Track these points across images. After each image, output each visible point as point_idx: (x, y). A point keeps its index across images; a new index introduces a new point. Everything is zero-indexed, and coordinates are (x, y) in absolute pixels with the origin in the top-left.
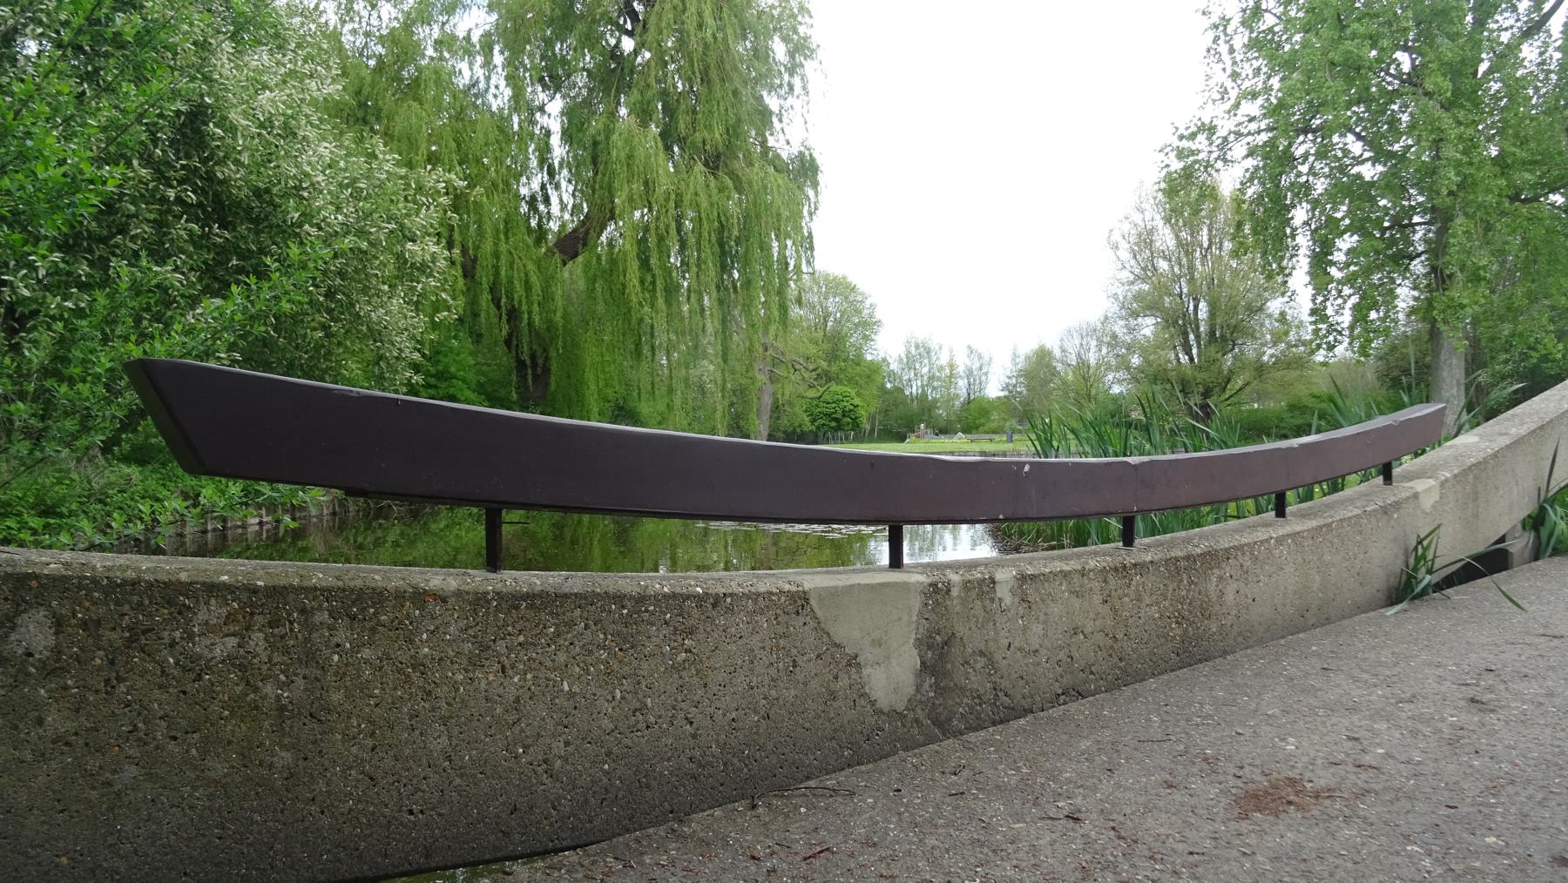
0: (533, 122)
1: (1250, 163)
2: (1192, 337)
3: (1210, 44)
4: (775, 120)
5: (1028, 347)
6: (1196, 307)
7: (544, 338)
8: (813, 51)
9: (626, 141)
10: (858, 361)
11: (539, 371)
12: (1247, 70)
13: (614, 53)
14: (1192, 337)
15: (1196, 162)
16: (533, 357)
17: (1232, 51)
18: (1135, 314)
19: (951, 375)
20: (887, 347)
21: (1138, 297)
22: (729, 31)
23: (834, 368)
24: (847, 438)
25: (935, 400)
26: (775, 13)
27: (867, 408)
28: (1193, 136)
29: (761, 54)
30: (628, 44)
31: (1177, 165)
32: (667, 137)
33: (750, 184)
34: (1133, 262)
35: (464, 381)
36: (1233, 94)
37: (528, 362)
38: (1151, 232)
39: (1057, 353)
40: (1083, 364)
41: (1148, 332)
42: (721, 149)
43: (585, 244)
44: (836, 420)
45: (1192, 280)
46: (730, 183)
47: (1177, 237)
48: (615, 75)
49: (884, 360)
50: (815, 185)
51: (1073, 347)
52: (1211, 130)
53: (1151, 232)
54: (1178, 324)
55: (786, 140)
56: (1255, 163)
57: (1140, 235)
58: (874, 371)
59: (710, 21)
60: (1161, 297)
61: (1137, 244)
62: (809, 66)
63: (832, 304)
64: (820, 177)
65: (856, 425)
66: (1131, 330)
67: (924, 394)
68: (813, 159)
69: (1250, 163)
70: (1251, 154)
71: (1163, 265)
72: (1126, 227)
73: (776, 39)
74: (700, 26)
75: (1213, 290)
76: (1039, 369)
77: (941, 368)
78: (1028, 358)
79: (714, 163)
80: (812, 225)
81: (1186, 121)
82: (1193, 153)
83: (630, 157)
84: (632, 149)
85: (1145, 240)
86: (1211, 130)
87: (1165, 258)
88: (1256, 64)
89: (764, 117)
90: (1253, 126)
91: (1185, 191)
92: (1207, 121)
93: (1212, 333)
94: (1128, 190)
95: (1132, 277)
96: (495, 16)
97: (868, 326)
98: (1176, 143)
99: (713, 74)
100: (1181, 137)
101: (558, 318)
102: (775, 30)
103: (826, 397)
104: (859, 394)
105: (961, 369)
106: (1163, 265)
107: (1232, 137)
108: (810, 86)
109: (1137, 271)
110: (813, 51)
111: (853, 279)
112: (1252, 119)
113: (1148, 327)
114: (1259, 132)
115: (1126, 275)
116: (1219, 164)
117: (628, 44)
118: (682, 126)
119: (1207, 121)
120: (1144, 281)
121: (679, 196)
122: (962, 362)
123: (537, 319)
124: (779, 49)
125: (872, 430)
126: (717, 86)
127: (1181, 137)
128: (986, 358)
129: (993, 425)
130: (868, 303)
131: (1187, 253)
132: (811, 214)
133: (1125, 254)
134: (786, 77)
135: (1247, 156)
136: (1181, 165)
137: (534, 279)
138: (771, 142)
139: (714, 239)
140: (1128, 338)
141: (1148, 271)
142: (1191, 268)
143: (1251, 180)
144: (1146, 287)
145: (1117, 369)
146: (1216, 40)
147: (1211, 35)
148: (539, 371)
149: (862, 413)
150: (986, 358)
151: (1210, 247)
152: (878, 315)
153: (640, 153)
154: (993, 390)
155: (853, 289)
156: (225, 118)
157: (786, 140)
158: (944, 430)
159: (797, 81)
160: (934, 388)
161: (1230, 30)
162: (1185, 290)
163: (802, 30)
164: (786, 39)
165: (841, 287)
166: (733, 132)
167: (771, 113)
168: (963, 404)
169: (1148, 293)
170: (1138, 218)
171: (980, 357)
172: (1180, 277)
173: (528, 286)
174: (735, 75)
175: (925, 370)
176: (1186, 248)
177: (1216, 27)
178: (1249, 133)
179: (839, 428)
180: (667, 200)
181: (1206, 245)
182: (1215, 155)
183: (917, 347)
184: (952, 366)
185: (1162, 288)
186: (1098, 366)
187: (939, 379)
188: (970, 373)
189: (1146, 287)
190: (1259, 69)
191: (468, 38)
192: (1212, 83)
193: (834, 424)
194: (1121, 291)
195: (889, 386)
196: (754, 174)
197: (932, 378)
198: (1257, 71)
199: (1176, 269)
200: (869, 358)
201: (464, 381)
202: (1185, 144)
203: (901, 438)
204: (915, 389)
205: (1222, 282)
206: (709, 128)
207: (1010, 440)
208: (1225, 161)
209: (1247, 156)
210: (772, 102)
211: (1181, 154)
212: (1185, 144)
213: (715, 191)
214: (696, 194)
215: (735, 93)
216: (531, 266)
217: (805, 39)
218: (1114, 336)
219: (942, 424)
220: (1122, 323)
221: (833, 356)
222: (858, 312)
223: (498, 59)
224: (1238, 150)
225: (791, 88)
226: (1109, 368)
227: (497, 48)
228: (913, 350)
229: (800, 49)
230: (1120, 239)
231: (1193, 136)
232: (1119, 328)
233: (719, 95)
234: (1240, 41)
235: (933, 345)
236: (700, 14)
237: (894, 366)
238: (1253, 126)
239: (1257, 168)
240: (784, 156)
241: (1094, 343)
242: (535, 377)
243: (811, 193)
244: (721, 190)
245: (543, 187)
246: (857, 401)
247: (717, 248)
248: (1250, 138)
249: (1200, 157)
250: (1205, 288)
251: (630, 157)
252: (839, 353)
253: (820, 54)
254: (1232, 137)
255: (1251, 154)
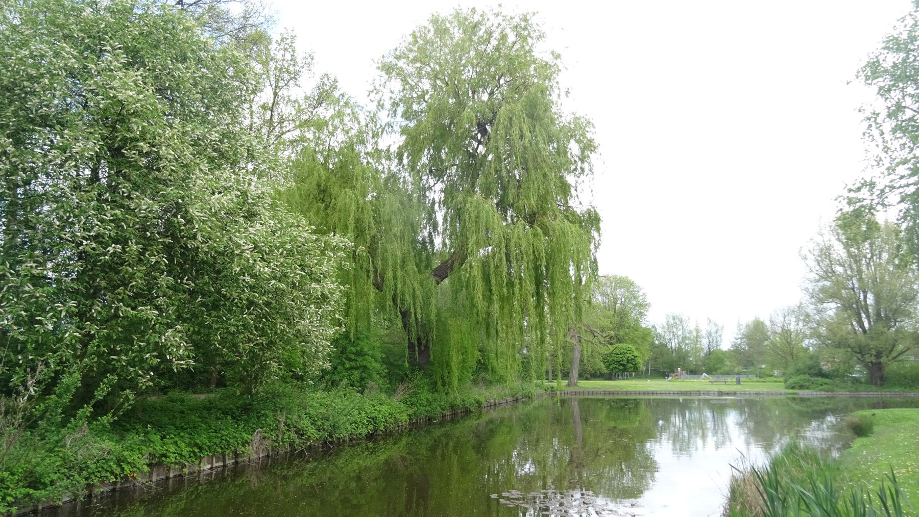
0: (424, 196)
1: (903, 206)
2: (863, 316)
3: (865, 129)
4: (572, 190)
5: (748, 319)
6: (865, 297)
7: (425, 327)
8: (595, 148)
9: (475, 207)
10: (636, 327)
11: (423, 348)
12: (896, 144)
13: (473, 155)
14: (863, 316)
15: (862, 206)
16: (419, 339)
17: (882, 134)
18: (822, 301)
19: (697, 336)
20: (654, 319)
21: (823, 290)
22: (540, 138)
23: (621, 333)
24: (631, 375)
25: (687, 352)
26: (572, 126)
27: (642, 359)
28: (859, 189)
29: (562, 152)
30: (481, 149)
31: (848, 209)
32: (503, 206)
33: (554, 231)
34: (818, 268)
35: (373, 356)
36: (887, 162)
37: (416, 343)
38: (829, 248)
39: (768, 323)
40: (786, 333)
41: (831, 313)
42: (535, 210)
43: (452, 270)
44: (623, 365)
45: (860, 280)
46: (540, 231)
47: (848, 251)
48: (472, 166)
49: (653, 327)
50: (598, 230)
51: (779, 320)
52: (872, 185)
53: (829, 248)
54: (853, 308)
55: (579, 203)
56: (906, 206)
57: (821, 250)
58: (646, 335)
59: (527, 134)
60: (839, 291)
61: (820, 256)
62: (593, 156)
63: (619, 292)
64: (601, 225)
65: (636, 368)
66: (819, 312)
67: (680, 347)
68: (596, 214)
69: (903, 206)
70: (902, 200)
71: (839, 269)
72: (811, 245)
73: (572, 141)
74: (522, 136)
75: (876, 286)
76: (756, 333)
77: (690, 332)
78: (747, 326)
79: (531, 219)
80: (597, 255)
81: (853, 180)
82: (859, 201)
83: (477, 217)
84: (479, 213)
85: (825, 253)
86: (872, 185)
87: (840, 265)
88: (902, 141)
89: (565, 189)
90: (904, 182)
91: (855, 224)
92: (868, 180)
93: (878, 314)
94: (814, 226)
95: (817, 277)
96: (404, 137)
97: (642, 306)
98: (846, 194)
99: (530, 165)
100: (850, 191)
101: (433, 317)
102: (572, 136)
103: (617, 351)
104: (637, 349)
105: (704, 333)
106: (839, 269)
107: (887, 190)
108: (594, 170)
109: (821, 273)
110: (595, 148)
111: (632, 278)
112: (902, 177)
113: (831, 308)
114: (908, 185)
115: (813, 276)
116: (879, 207)
117: (481, 149)
118: (511, 197)
119: (868, 180)
120: (826, 279)
121: (508, 240)
122: (704, 329)
123: (419, 317)
124: (574, 148)
125: (647, 370)
126: (533, 172)
127: (850, 191)
128: (720, 326)
129: (726, 369)
130: (641, 293)
131: (856, 261)
132: (596, 248)
133: (812, 263)
134: (579, 163)
135: (900, 202)
136: (852, 208)
137: (418, 293)
138: (571, 203)
139: (531, 266)
140: (817, 317)
141: (828, 274)
142: (860, 272)
143: (905, 217)
144: (828, 284)
145: (811, 337)
146: (870, 126)
147: (866, 124)
148: (423, 348)
149: (639, 360)
150: (720, 326)
151: (872, 257)
152: (648, 300)
153: (483, 215)
154: (726, 345)
155: (632, 284)
156: (187, 212)
157: (579, 203)
158: (694, 372)
159: (586, 166)
160: (687, 344)
161: (879, 120)
162: (856, 286)
163: (589, 135)
164: (578, 142)
165: (624, 283)
166: (543, 199)
167: (569, 186)
168: (706, 355)
169: (830, 288)
170: (819, 239)
171: (716, 325)
172: (852, 277)
173: (414, 297)
174: (544, 165)
175: (680, 333)
176: (856, 259)
177: (869, 119)
178: (900, 187)
179: (625, 370)
180: (500, 243)
181: (869, 256)
182: (876, 201)
183: (674, 319)
184: (697, 331)
185: (839, 284)
186: (797, 335)
187: (689, 339)
188: (710, 335)
189: (828, 284)
190: (904, 144)
191: (388, 150)
192: (870, 155)
193: (621, 368)
194: (811, 287)
195: (657, 342)
196: (558, 224)
197: (684, 338)
198: (903, 146)
199: (849, 272)
200: (644, 326)
201: (373, 356)
202: (852, 195)
203: (664, 375)
204: (674, 344)
205: (882, 279)
206: (528, 197)
207: (738, 382)
208: (884, 205)
209: (900, 202)
210: (570, 179)
211: (850, 202)
212: (852, 195)
213: (531, 237)
214: (519, 239)
215: (545, 175)
216: (416, 285)
217: (590, 141)
218: (808, 315)
219: (693, 367)
220: (813, 307)
221: (620, 325)
222: (635, 298)
223: (405, 161)
224: (893, 198)
225: (583, 170)
226: (805, 336)
227: (406, 154)
228: (671, 321)
229: (588, 147)
230: (808, 253)
231: (859, 189)
232: (811, 309)
233: (533, 177)
234: (888, 126)
235: (684, 318)
236: (521, 129)
237: (659, 331)
238: (904, 182)
239: (908, 210)
240: (579, 212)
241: (793, 319)
242: (420, 353)
243: (595, 234)
244: (535, 235)
245: (430, 234)
246: (636, 353)
247: (533, 272)
248: (901, 190)
249: (865, 203)
250: (870, 285)
251: (477, 217)
252: (623, 323)
253: (600, 149)
254: (887, 190)
255: (902, 200)
